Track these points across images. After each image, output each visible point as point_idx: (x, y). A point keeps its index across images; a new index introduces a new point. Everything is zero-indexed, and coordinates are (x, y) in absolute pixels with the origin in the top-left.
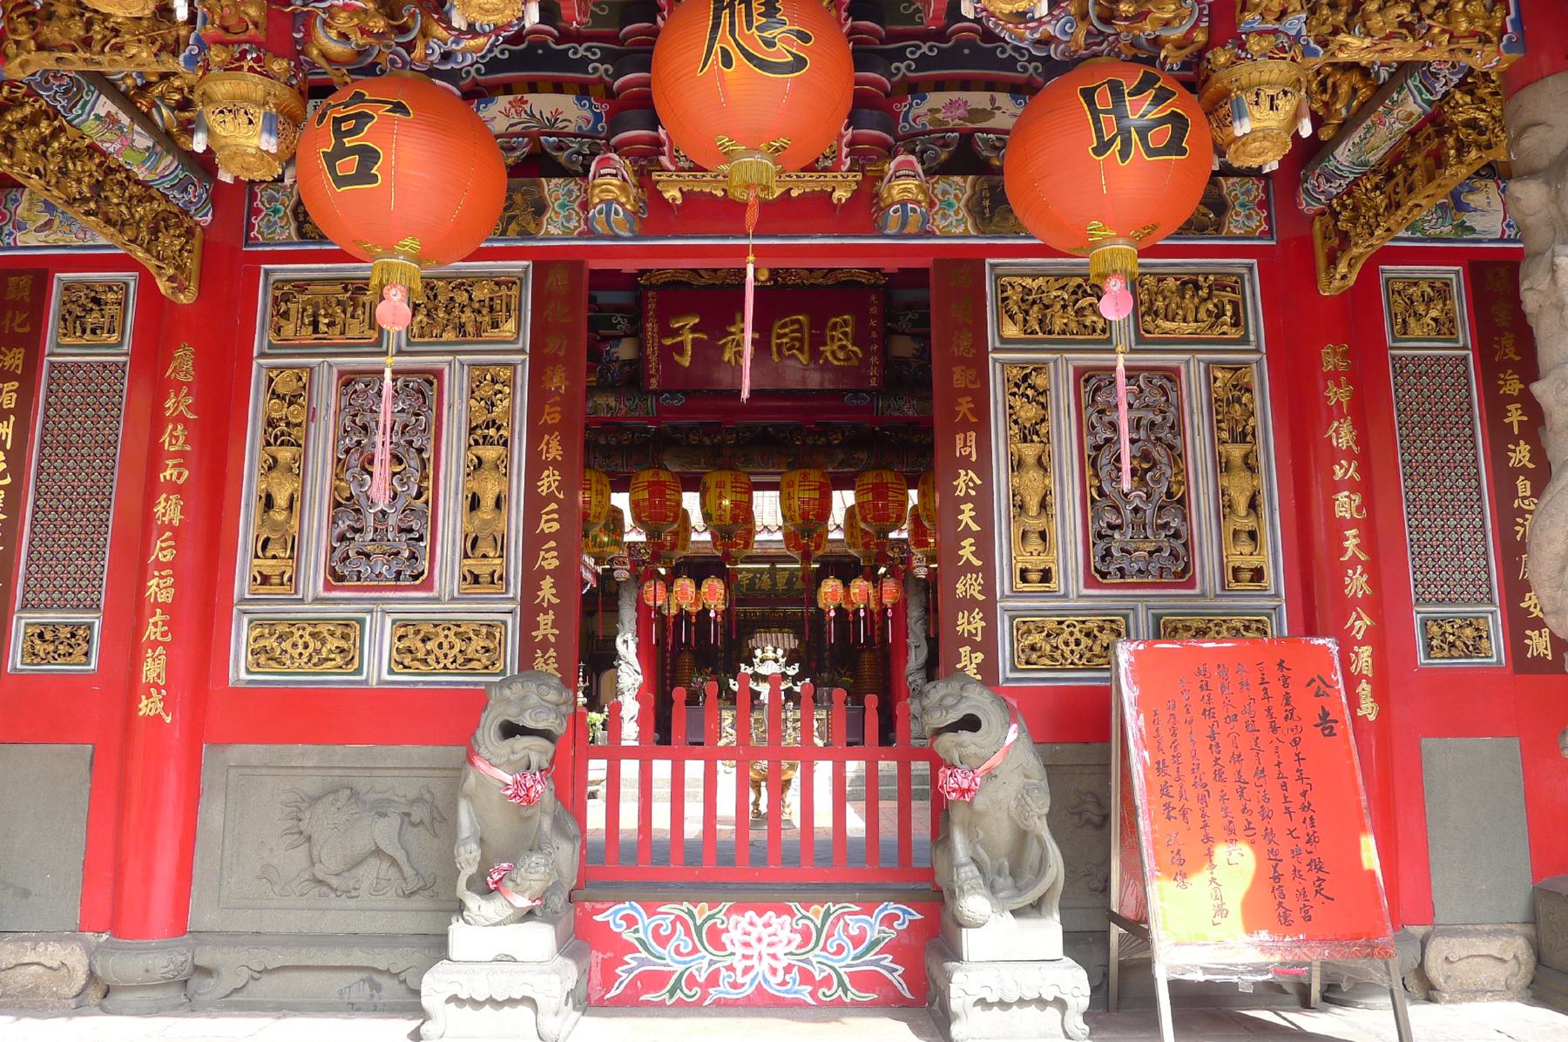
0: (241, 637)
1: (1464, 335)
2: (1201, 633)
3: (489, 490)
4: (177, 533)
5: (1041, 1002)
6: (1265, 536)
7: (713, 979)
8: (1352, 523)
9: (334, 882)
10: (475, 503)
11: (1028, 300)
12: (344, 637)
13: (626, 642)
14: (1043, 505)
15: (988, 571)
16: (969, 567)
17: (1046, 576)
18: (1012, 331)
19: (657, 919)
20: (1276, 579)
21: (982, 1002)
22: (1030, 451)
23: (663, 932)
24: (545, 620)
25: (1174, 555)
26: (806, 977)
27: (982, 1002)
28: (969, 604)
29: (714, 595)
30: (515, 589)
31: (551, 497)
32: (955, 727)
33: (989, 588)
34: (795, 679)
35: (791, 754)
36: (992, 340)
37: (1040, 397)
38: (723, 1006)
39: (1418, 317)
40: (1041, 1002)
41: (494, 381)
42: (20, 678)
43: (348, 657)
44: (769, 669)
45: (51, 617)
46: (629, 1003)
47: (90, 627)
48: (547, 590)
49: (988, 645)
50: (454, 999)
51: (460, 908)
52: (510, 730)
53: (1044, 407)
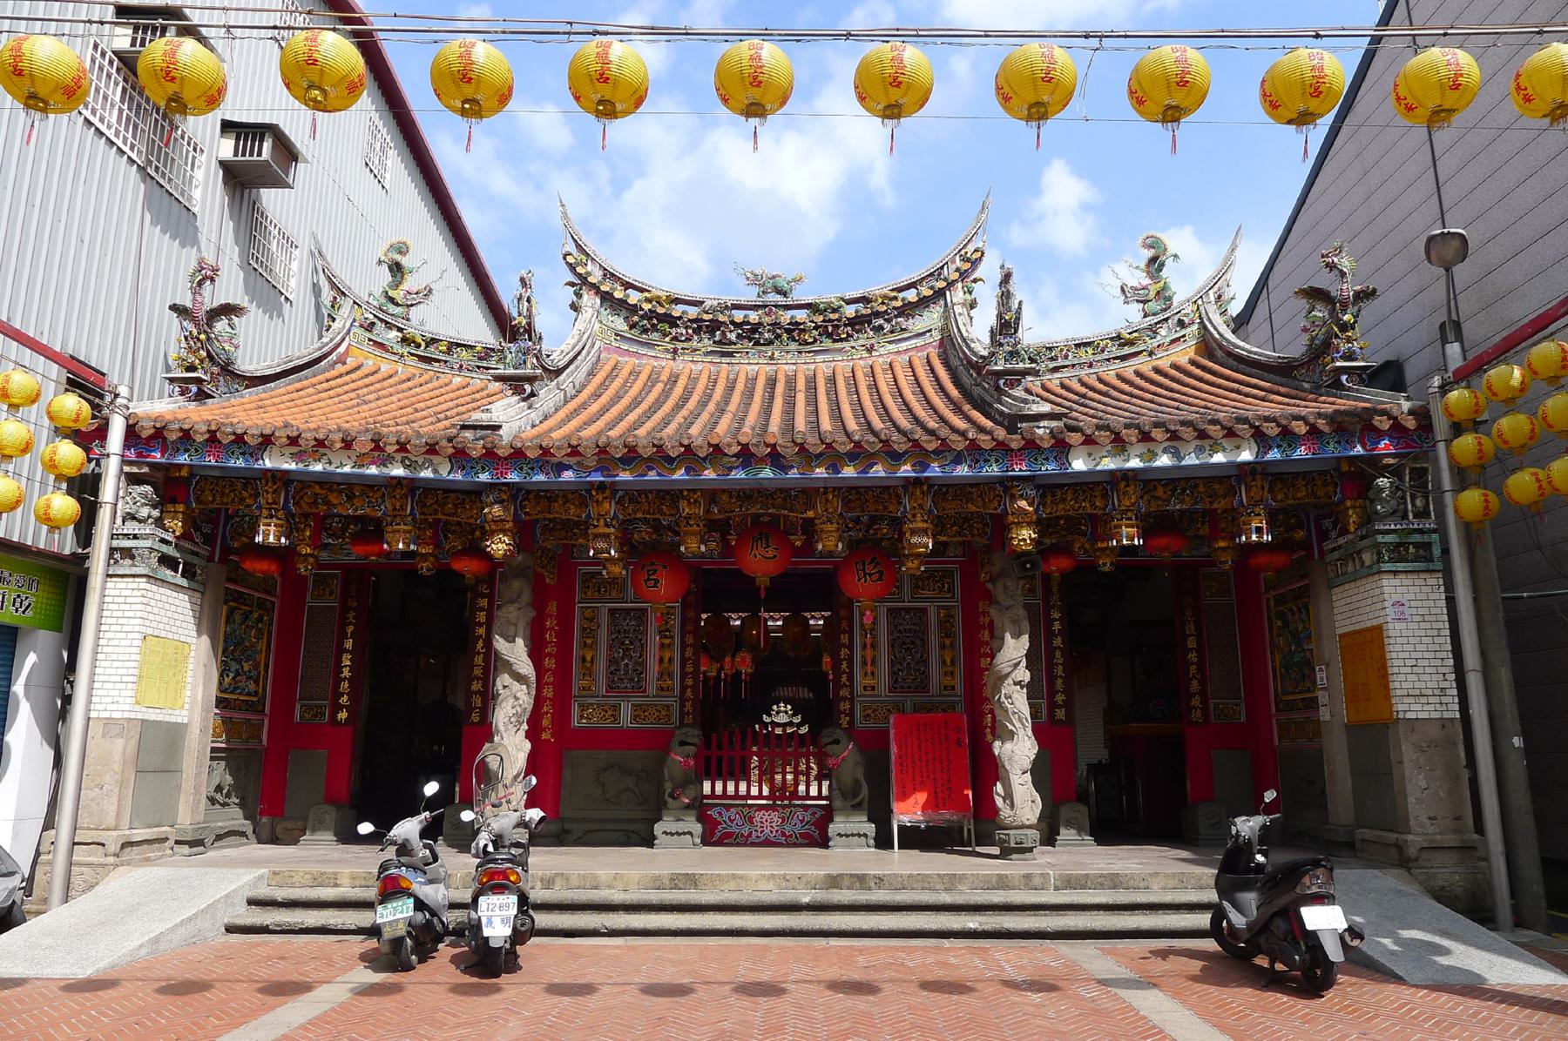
0: (575, 709)
1: (1039, 594)
2: (930, 710)
3: (667, 655)
4: (554, 672)
5: (859, 835)
6: (957, 672)
7: (750, 835)
10: (661, 660)
14: (873, 662)
15: (852, 686)
17: (873, 688)
20: (959, 689)
29: (745, 665)
30: (677, 692)
33: (852, 693)
34: (799, 725)
35: (802, 773)
38: (753, 844)
40: (859, 835)
43: (616, 718)
44: (782, 719)
46: (719, 843)
48: (689, 693)
49: (851, 714)
51: (665, 803)
52: (682, 743)
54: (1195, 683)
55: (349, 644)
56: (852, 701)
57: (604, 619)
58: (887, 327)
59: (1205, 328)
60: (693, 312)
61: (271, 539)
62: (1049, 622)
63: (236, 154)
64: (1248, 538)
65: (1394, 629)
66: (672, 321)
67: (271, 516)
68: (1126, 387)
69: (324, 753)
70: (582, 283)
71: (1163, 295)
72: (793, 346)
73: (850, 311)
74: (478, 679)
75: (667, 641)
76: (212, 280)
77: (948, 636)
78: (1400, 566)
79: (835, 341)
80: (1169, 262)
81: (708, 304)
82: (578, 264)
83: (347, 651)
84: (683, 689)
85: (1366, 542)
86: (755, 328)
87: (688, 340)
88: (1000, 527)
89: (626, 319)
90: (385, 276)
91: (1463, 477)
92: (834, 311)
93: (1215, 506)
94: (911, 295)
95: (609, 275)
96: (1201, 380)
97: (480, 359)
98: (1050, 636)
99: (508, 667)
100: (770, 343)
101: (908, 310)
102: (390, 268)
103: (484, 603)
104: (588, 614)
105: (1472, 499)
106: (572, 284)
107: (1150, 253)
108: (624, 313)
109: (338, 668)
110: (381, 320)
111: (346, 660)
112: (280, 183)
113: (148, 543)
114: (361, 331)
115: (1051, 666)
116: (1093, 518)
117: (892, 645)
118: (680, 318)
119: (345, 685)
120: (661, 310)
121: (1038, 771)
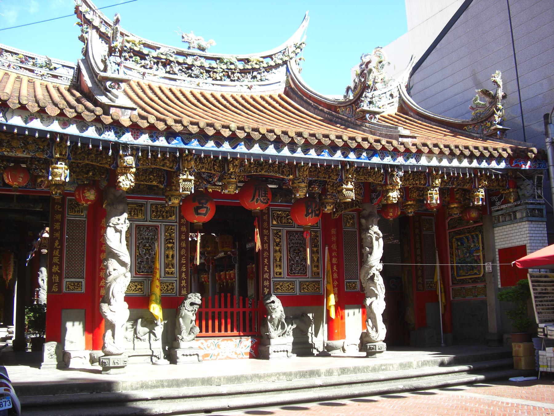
1: (356, 226)
5: (284, 351)
7: (218, 355)
8: (335, 264)
9: (141, 338)
10: (167, 256)
11: (278, 216)
12: (142, 286)
13: (43, 280)
14: (280, 259)
16: (266, 272)
17: (280, 274)
18: (275, 223)
19: (207, 343)
21: (274, 352)
22: (278, 248)
23: (209, 346)
24: (184, 282)
25: (304, 270)
26: (236, 353)
27: (274, 352)
28: (266, 279)
31: (184, 255)
32: (270, 303)
33: (270, 276)
36: (271, 225)
37: (280, 237)
39: (349, 222)
41: (171, 229)
42: (66, 294)
45: (73, 280)
47: (82, 282)
48: (183, 275)
50: (183, 355)
52: (192, 304)
53: (280, 239)
54: (420, 271)
56: (269, 280)
58: (259, 77)
59: (403, 100)
60: (154, 54)
64: (427, 202)
66: (143, 56)
68: (225, 102)
72: (210, 80)
73: (241, 66)
74: (56, 264)
75: (170, 245)
77: (316, 246)
78: (534, 219)
79: (232, 80)
81: (161, 51)
84: (181, 273)
86: (190, 67)
87: (151, 68)
92: (231, 63)
93: (465, 187)
96: (286, 109)
99: (116, 256)
100: (197, 77)
101: (269, 69)
103: (58, 217)
117: (289, 251)
118: (148, 55)
120: (136, 49)
121: (386, 316)
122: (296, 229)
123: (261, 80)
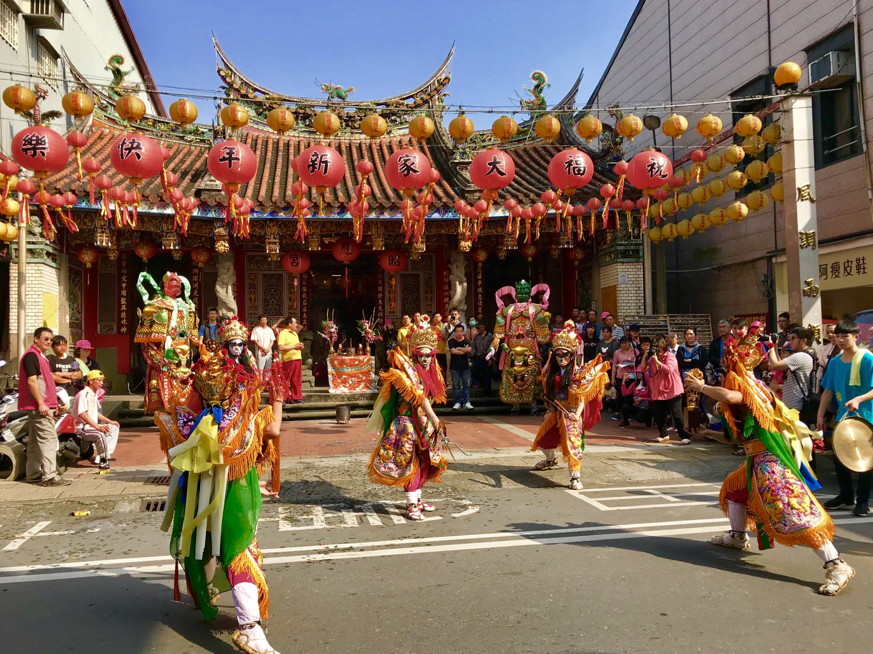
15: (384, 312)
55: (124, 293)
57: (260, 278)
58: (398, 119)
61: (104, 244)
62: (477, 280)
63: (32, 11)
65: (621, 287)
67: (103, 232)
69: (115, 349)
70: (230, 87)
71: (542, 104)
76: (44, 98)
78: (625, 260)
80: (545, 89)
82: (227, 75)
83: (123, 296)
85: (613, 249)
88: (455, 239)
89: (255, 110)
90: (110, 75)
91: (652, 223)
94: (410, 102)
95: (244, 83)
97: (173, 130)
98: (477, 286)
102: (113, 72)
104: (252, 277)
105: (655, 233)
106: (223, 88)
107: (535, 83)
108: (254, 107)
109: (120, 306)
110: (111, 105)
111: (123, 301)
112: (53, 25)
113: (42, 246)
114: (99, 111)
115: (476, 301)
116: (497, 237)
119: (123, 315)
122: (410, 272)
123: (401, 123)
